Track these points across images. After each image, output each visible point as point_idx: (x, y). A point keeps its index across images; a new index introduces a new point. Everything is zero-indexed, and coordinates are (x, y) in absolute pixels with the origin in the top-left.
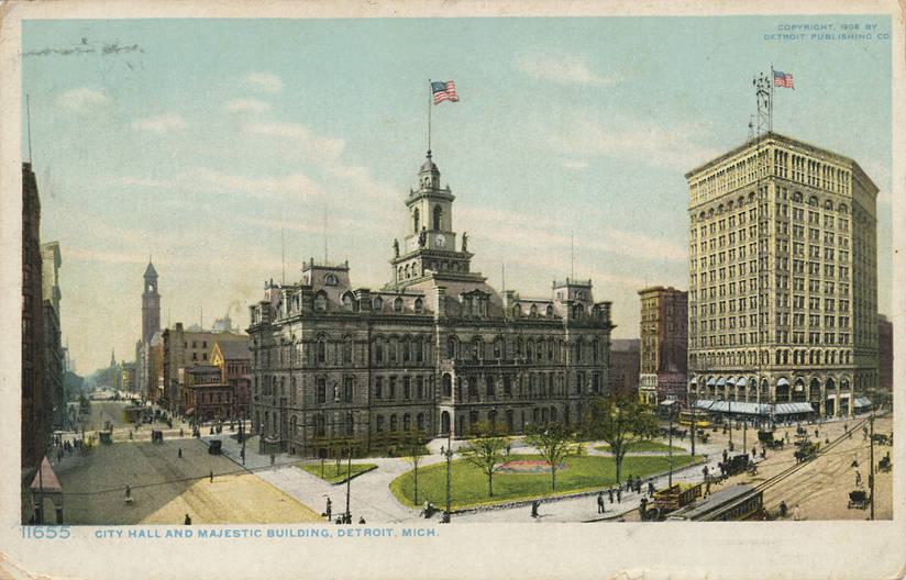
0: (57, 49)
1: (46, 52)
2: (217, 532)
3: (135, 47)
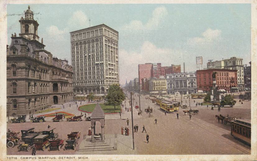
0: (17, 14)
1: (14, 15)
2: (44, 158)
3: (39, 13)
